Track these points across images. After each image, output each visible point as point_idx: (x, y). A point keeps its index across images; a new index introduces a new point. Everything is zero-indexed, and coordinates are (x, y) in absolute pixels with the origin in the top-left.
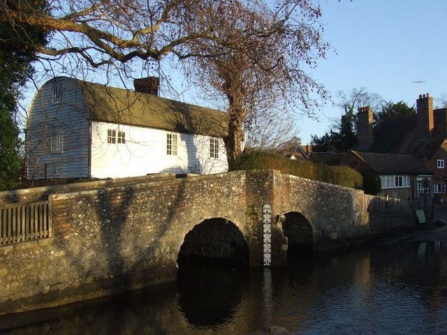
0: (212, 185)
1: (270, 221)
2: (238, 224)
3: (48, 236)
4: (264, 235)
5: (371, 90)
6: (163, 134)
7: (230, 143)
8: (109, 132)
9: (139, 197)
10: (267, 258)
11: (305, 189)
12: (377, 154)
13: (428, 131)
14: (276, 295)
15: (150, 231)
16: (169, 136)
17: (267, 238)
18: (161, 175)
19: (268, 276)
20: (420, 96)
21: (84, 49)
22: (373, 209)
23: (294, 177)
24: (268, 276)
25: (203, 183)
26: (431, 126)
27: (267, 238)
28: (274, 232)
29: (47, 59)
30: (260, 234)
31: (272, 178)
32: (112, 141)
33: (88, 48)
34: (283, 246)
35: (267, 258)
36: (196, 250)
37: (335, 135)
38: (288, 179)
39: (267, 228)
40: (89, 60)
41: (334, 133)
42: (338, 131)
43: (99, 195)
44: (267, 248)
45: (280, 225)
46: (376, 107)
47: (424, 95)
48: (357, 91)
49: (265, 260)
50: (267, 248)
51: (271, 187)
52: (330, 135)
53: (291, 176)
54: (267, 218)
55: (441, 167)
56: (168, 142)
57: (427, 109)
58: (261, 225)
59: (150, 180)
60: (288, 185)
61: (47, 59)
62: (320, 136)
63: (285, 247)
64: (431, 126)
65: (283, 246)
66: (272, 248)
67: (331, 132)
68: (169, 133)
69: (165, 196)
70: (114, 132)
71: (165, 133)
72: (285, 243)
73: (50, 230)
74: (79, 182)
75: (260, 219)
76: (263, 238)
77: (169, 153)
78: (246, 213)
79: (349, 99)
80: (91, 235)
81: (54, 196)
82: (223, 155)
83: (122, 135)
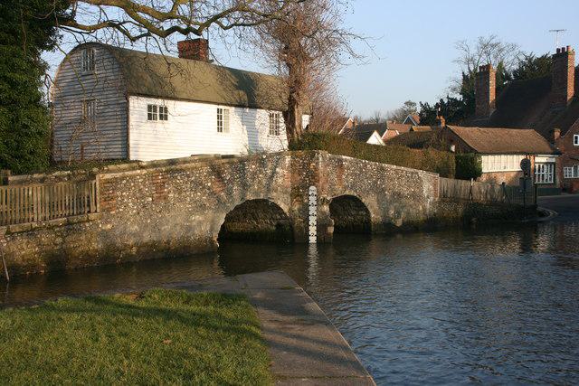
1: (315, 203)
2: (282, 206)
3: (96, 212)
5: (504, 39)
6: (212, 109)
7: (290, 117)
8: (150, 107)
9: (179, 178)
11: (361, 171)
16: (219, 111)
20: (558, 50)
21: (121, 24)
25: (244, 165)
26: (571, 91)
27: (313, 220)
28: (321, 215)
29: (80, 33)
33: (124, 22)
34: (329, 228)
37: (453, 102)
38: (341, 160)
39: (312, 210)
40: (125, 33)
41: (452, 99)
42: (459, 97)
44: (313, 230)
45: (326, 208)
46: (512, 65)
48: (486, 39)
50: (313, 230)
53: (344, 157)
54: (313, 200)
56: (219, 117)
57: (566, 67)
59: (195, 161)
61: (80, 33)
62: (432, 104)
63: (331, 230)
64: (571, 91)
65: (329, 228)
66: (317, 231)
67: (448, 97)
70: (155, 107)
71: (215, 107)
72: (330, 225)
73: (98, 206)
74: (286, 121)
76: (309, 220)
77: (220, 130)
78: (291, 195)
79: (473, 51)
81: (101, 176)
82: (284, 136)
83: (164, 110)
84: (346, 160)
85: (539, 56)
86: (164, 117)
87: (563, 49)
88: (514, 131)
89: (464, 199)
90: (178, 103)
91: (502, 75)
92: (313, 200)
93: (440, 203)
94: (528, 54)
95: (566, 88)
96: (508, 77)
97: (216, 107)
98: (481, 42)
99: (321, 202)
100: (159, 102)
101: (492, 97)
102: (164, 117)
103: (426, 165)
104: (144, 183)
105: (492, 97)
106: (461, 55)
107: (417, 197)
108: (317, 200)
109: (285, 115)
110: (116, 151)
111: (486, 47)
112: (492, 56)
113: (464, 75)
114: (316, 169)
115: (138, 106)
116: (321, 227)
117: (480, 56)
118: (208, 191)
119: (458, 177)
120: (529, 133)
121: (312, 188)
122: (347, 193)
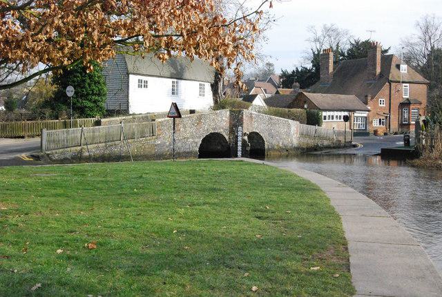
5: (341, 26)
12: (324, 95)
13: (375, 75)
16: (173, 82)
17: (240, 144)
27: (240, 144)
30: (236, 143)
32: (140, 86)
37: (305, 71)
39: (240, 138)
43: (347, 121)
44: (240, 148)
45: (246, 138)
46: (345, 47)
48: (329, 25)
50: (240, 148)
51: (242, 118)
52: (300, 70)
54: (240, 133)
55: (382, 105)
58: (237, 137)
60: (251, 117)
62: (290, 71)
63: (248, 149)
68: (201, 83)
71: (171, 81)
77: (173, 93)
79: (319, 34)
85: (364, 41)
86: (146, 86)
88: (343, 96)
90: (183, 81)
91: (337, 53)
94: (356, 39)
95: (375, 69)
96: (342, 54)
97: (198, 83)
98: (325, 28)
100: (144, 78)
101: (331, 69)
102: (146, 86)
103: (295, 118)
105: (331, 69)
106: (312, 36)
107: (288, 134)
109: (212, 86)
110: (123, 107)
111: (328, 31)
112: (332, 38)
113: (314, 53)
115: (133, 80)
117: (325, 37)
119: (308, 123)
120: (352, 97)
121: (240, 127)
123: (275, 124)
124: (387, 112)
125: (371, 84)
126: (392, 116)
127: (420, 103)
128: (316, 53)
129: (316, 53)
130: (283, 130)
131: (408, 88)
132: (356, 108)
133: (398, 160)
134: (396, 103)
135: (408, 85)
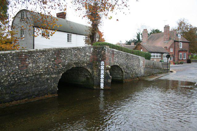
0: (76, 52)
1: (104, 69)
4: (101, 84)
10: (102, 86)
14: (106, 98)
15: (42, 72)
17: (102, 76)
18: (165, 74)
19: (102, 94)
20: (165, 26)
22: (147, 67)
23: (116, 50)
24: (102, 94)
27: (102, 76)
30: (99, 75)
31: (105, 49)
35: (102, 86)
36: (98, 56)
39: (102, 72)
44: (102, 81)
47: (167, 26)
49: (101, 86)
50: (102, 81)
54: (102, 67)
58: (100, 70)
63: (110, 81)
68: (69, 34)
69: (51, 55)
75: (99, 68)
77: (68, 41)
80: (6, 74)
84: (115, 51)
87: (167, 26)
89: (6, 15)
92: (102, 67)
93: (145, 68)
94: (153, 29)
99: (106, 69)
100: (70, 34)
104: (12, 59)
108: (104, 68)
114: (104, 54)
116: (106, 77)
118: (52, 63)
121: (102, 62)
122: (115, 64)
123: (130, 59)
124: (174, 54)
125: (166, 42)
126: (175, 56)
127: (187, 51)
128: (138, 34)
129: (138, 34)
130: (136, 63)
131: (182, 44)
132: (164, 52)
133: (7, 9)
134: (177, 50)
135: (182, 43)
